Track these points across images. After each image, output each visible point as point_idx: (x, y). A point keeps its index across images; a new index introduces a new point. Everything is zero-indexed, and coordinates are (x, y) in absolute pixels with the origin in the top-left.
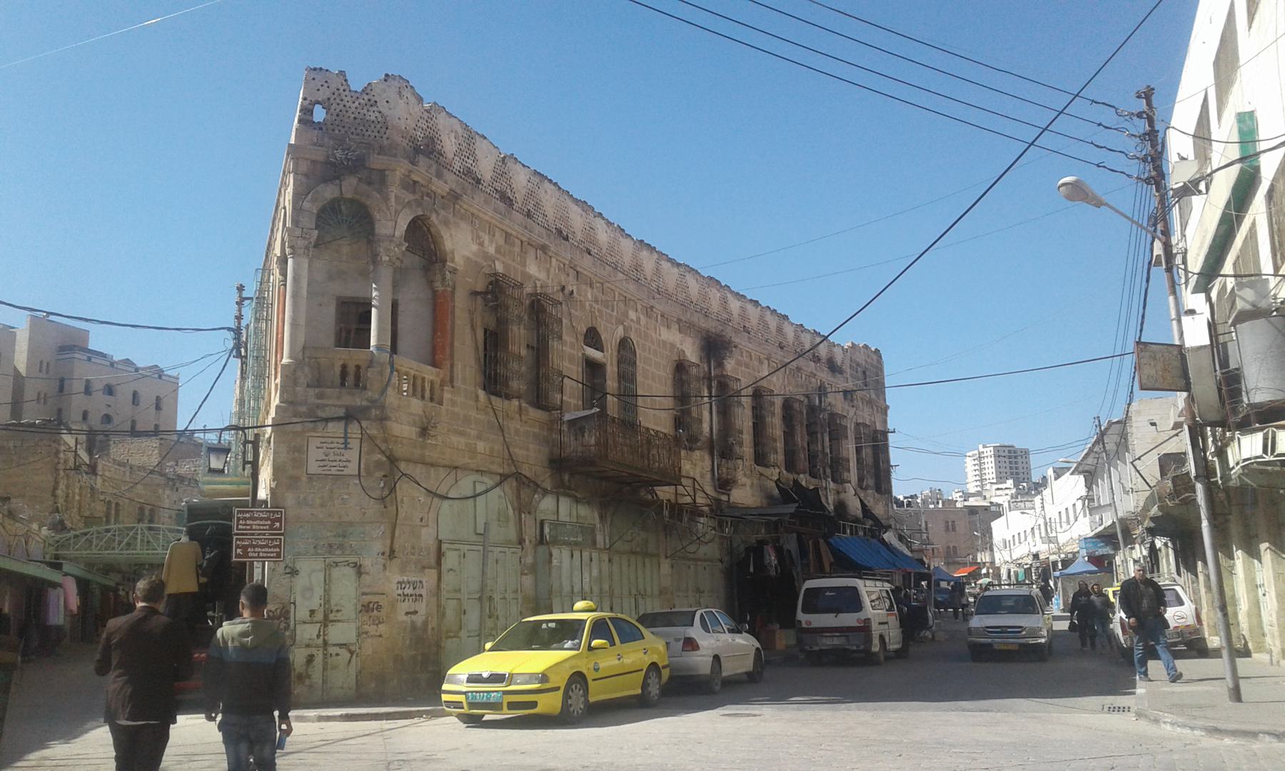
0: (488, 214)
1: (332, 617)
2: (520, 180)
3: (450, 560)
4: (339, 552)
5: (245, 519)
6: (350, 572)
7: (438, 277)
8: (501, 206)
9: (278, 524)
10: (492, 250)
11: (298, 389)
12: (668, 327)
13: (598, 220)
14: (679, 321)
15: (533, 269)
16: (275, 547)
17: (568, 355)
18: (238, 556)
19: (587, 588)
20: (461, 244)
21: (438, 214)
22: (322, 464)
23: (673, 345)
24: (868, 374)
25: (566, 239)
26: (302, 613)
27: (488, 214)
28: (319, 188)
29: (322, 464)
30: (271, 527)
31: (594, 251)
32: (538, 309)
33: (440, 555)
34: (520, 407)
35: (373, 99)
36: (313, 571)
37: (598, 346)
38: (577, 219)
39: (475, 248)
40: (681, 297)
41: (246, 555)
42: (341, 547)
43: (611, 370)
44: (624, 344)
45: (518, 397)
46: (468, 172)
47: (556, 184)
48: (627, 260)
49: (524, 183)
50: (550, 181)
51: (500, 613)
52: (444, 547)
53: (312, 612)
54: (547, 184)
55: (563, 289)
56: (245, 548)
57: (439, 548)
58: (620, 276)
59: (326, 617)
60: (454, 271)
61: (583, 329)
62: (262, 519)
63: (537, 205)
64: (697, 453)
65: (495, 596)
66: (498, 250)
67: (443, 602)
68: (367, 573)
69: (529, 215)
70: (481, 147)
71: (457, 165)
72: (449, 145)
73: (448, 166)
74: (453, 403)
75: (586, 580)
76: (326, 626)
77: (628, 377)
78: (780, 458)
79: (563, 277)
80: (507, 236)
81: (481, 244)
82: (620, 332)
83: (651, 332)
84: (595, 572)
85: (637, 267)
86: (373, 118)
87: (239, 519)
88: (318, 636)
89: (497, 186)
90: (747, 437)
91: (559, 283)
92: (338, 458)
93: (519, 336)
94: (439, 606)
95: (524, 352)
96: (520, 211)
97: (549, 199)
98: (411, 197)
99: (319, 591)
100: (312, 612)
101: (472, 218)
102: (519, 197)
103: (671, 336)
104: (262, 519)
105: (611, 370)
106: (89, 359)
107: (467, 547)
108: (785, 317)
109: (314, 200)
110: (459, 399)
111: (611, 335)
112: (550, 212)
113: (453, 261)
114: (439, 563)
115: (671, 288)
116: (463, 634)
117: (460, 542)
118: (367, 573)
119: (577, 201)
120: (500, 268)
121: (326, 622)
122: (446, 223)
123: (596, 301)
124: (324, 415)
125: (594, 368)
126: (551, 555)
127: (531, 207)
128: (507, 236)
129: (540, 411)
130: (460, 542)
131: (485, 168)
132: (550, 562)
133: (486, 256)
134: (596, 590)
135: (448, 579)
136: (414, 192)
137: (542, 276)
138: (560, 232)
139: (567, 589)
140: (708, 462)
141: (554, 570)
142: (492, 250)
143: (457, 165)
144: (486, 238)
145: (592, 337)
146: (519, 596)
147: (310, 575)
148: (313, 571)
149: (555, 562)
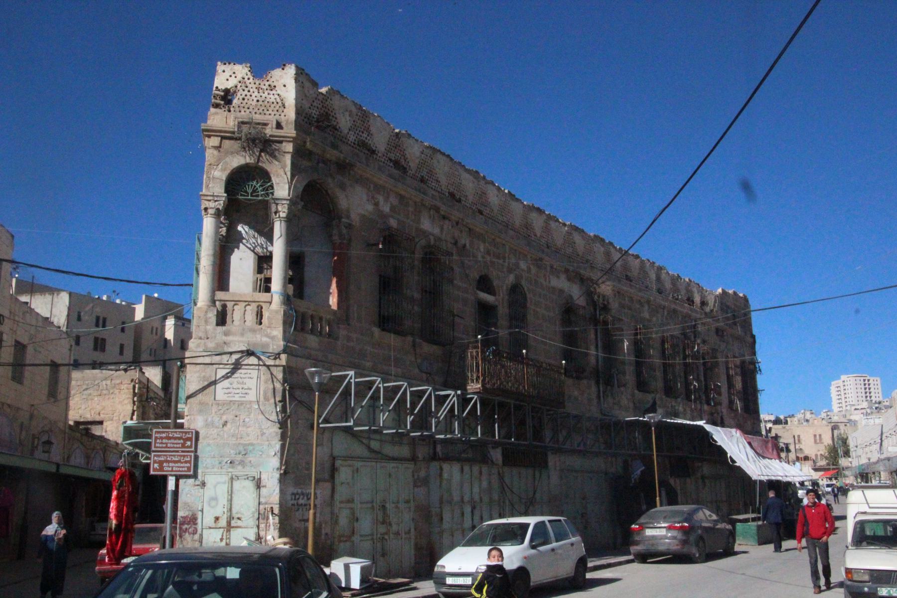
0: (382, 179)
1: (233, 523)
2: (413, 152)
3: (344, 474)
4: (240, 467)
5: (162, 438)
6: (250, 485)
7: (335, 232)
8: (395, 172)
9: (189, 443)
10: (387, 209)
11: (208, 327)
12: (558, 277)
13: (490, 187)
14: (567, 271)
15: (426, 224)
16: (186, 462)
17: (461, 297)
18: (155, 470)
19: (477, 498)
20: (356, 203)
21: (334, 179)
22: (227, 391)
23: (561, 291)
24: (736, 315)
25: (459, 201)
26: (207, 519)
27: (382, 179)
28: (227, 159)
29: (227, 391)
30: (183, 446)
31: (486, 211)
32: (432, 259)
33: (333, 470)
34: (414, 341)
35: (273, 85)
36: (218, 483)
37: (490, 290)
38: (469, 185)
39: (370, 207)
40: (569, 250)
41: (161, 469)
42: (242, 463)
43: (503, 311)
44: (515, 289)
45: (412, 334)
46: (363, 145)
47: (448, 156)
48: (518, 221)
49: (418, 154)
50: (444, 154)
51: (393, 519)
52: (338, 463)
53: (217, 519)
54: (439, 156)
55: (456, 243)
56: (161, 463)
57: (333, 465)
58: (511, 233)
59: (229, 523)
60: (349, 226)
61: (475, 275)
62: (175, 438)
63: (431, 172)
64: (585, 381)
65: (387, 505)
66: (393, 208)
67: (336, 511)
68: (265, 486)
69: (422, 180)
70: (375, 126)
71: (352, 138)
72: (344, 122)
73: (343, 139)
74: (349, 339)
75: (476, 490)
76: (228, 531)
77: (518, 316)
78: (660, 384)
79: (457, 234)
80: (401, 198)
81: (376, 204)
82: (511, 278)
83: (542, 280)
84: (485, 484)
85: (528, 226)
86: (273, 100)
87: (156, 438)
88: (221, 540)
89: (392, 156)
90: (630, 370)
91: (454, 238)
92: (240, 386)
93: (413, 285)
94: (332, 513)
95: (417, 295)
96: (414, 177)
97: (441, 168)
98: (308, 164)
99: (223, 501)
100: (217, 519)
101: (362, 181)
102: (413, 165)
103: (561, 283)
104: (175, 438)
105: (503, 311)
106: (183, 325)
107: (360, 464)
108: (611, 244)
109: (223, 170)
110: (354, 336)
111: (503, 281)
112: (443, 180)
113: (348, 217)
114: (332, 477)
115: (559, 242)
116: (356, 539)
117: (352, 458)
118: (265, 486)
119: (469, 171)
120: (393, 223)
121: (229, 527)
122: (343, 187)
123: (488, 253)
124: (230, 350)
125: (486, 311)
126: (441, 469)
127: (424, 173)
128: (401, 198)
129: (435, 347)
130: (352, 458)
131: (380, 142)
132: (441, 475)
133: (384, 216)
134: (486, 499)
135: (342, 492)
136: (310, 160)
137: (436, 231)
138: (452, 195)
139: (456, 498)
140: (594, 389)
141: (444, 482)
142: (387, 209)
143: (352, 138)
144: (381, 199)
145: (484, 283)
146: (412, 504)
147: (215, 487)
148: (218, 483)
149: (445, 476)
